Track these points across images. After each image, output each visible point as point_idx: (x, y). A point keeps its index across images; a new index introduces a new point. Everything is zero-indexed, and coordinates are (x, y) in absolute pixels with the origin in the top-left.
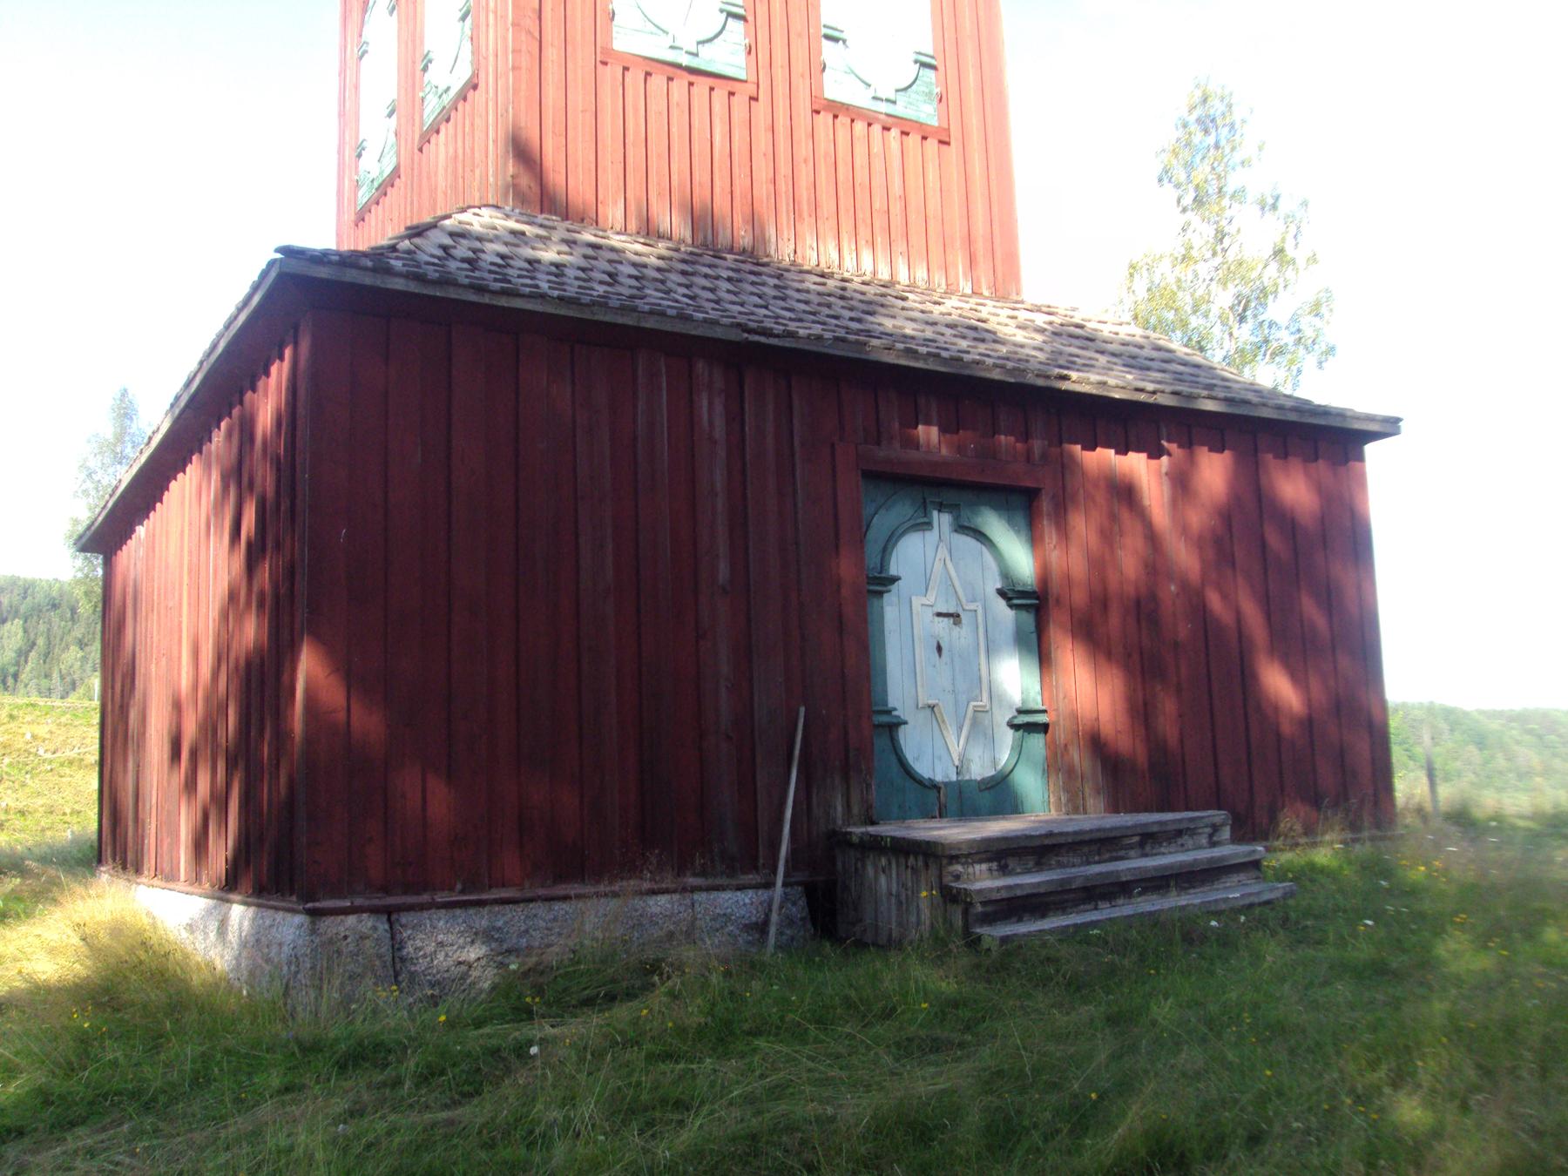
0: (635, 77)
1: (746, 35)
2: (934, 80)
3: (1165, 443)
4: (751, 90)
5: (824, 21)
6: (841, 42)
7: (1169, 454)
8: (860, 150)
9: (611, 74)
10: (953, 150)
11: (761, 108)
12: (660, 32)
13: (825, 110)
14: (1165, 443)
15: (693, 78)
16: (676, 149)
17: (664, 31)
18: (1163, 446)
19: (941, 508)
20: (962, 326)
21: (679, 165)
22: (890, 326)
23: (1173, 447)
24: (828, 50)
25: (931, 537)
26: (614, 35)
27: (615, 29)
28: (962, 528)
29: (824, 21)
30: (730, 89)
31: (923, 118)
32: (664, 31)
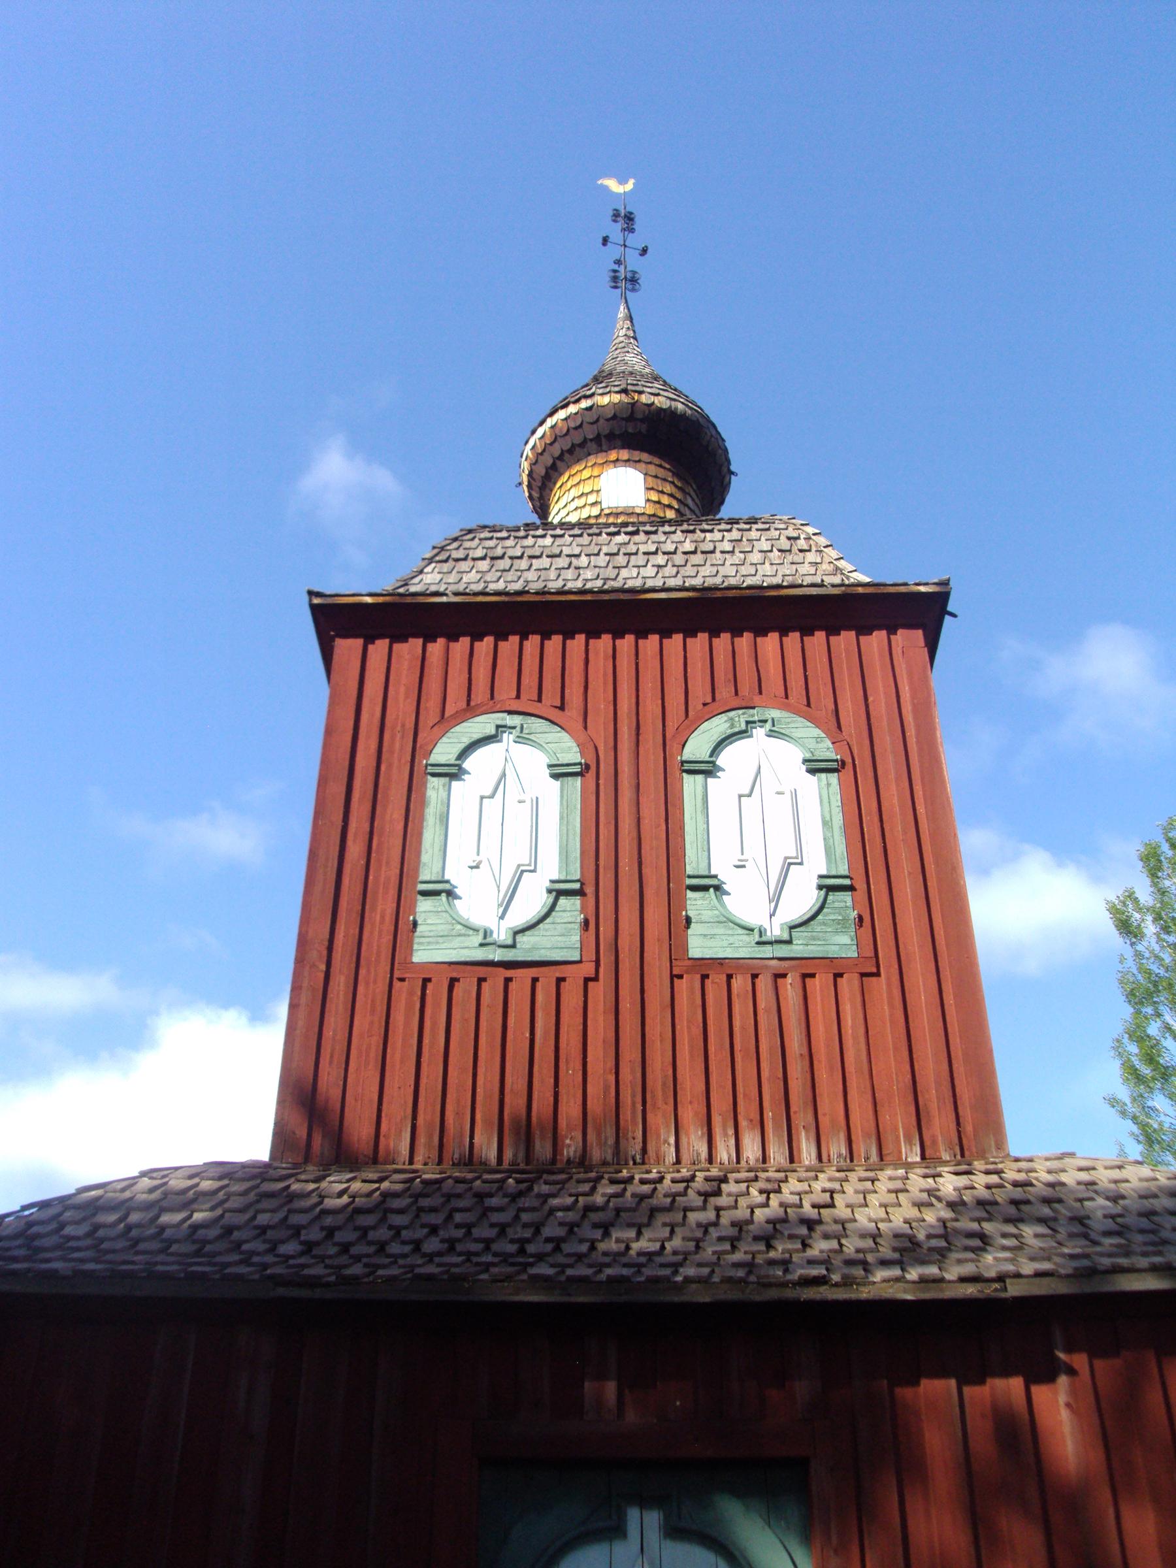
0: (819, 985)
1: (583, 909)
2: (849, 903)
3: (1062, 1355)
4: (588, 969)
5: (689, 870)
6: (712, 890)
7: (1071, 1372)
8: (741, 1009)
9: (687, 988)
10: (883, 988)
11: (600, 992)
12: (471, 932)
13: (687, 972)
14: (1062, 1355)
15: (509, 973)
16: (740, 1068)
17: (474, 930)
18: (1058, 1359)
19: (644, 1503)
20: (361, 1196)
21: (516, 1081)
22: (852, 1249)
23: (1079, 1361)
24: (696, 904)
25: (624, 1551)
26: (415, 947)
27: (416, 940)
28: (675, 1531)
29: (689, 870)
30: (558, 975)
31: (833, 951)
32: (474, 930)
